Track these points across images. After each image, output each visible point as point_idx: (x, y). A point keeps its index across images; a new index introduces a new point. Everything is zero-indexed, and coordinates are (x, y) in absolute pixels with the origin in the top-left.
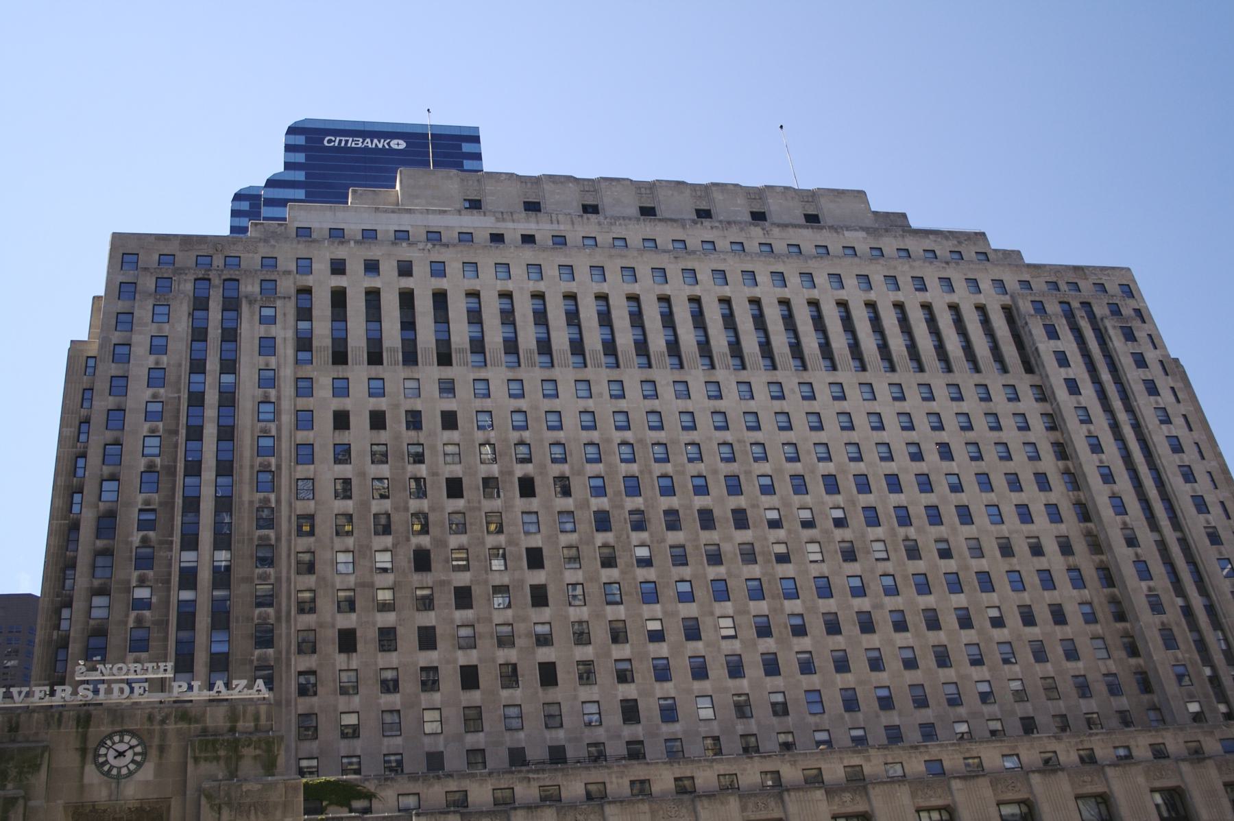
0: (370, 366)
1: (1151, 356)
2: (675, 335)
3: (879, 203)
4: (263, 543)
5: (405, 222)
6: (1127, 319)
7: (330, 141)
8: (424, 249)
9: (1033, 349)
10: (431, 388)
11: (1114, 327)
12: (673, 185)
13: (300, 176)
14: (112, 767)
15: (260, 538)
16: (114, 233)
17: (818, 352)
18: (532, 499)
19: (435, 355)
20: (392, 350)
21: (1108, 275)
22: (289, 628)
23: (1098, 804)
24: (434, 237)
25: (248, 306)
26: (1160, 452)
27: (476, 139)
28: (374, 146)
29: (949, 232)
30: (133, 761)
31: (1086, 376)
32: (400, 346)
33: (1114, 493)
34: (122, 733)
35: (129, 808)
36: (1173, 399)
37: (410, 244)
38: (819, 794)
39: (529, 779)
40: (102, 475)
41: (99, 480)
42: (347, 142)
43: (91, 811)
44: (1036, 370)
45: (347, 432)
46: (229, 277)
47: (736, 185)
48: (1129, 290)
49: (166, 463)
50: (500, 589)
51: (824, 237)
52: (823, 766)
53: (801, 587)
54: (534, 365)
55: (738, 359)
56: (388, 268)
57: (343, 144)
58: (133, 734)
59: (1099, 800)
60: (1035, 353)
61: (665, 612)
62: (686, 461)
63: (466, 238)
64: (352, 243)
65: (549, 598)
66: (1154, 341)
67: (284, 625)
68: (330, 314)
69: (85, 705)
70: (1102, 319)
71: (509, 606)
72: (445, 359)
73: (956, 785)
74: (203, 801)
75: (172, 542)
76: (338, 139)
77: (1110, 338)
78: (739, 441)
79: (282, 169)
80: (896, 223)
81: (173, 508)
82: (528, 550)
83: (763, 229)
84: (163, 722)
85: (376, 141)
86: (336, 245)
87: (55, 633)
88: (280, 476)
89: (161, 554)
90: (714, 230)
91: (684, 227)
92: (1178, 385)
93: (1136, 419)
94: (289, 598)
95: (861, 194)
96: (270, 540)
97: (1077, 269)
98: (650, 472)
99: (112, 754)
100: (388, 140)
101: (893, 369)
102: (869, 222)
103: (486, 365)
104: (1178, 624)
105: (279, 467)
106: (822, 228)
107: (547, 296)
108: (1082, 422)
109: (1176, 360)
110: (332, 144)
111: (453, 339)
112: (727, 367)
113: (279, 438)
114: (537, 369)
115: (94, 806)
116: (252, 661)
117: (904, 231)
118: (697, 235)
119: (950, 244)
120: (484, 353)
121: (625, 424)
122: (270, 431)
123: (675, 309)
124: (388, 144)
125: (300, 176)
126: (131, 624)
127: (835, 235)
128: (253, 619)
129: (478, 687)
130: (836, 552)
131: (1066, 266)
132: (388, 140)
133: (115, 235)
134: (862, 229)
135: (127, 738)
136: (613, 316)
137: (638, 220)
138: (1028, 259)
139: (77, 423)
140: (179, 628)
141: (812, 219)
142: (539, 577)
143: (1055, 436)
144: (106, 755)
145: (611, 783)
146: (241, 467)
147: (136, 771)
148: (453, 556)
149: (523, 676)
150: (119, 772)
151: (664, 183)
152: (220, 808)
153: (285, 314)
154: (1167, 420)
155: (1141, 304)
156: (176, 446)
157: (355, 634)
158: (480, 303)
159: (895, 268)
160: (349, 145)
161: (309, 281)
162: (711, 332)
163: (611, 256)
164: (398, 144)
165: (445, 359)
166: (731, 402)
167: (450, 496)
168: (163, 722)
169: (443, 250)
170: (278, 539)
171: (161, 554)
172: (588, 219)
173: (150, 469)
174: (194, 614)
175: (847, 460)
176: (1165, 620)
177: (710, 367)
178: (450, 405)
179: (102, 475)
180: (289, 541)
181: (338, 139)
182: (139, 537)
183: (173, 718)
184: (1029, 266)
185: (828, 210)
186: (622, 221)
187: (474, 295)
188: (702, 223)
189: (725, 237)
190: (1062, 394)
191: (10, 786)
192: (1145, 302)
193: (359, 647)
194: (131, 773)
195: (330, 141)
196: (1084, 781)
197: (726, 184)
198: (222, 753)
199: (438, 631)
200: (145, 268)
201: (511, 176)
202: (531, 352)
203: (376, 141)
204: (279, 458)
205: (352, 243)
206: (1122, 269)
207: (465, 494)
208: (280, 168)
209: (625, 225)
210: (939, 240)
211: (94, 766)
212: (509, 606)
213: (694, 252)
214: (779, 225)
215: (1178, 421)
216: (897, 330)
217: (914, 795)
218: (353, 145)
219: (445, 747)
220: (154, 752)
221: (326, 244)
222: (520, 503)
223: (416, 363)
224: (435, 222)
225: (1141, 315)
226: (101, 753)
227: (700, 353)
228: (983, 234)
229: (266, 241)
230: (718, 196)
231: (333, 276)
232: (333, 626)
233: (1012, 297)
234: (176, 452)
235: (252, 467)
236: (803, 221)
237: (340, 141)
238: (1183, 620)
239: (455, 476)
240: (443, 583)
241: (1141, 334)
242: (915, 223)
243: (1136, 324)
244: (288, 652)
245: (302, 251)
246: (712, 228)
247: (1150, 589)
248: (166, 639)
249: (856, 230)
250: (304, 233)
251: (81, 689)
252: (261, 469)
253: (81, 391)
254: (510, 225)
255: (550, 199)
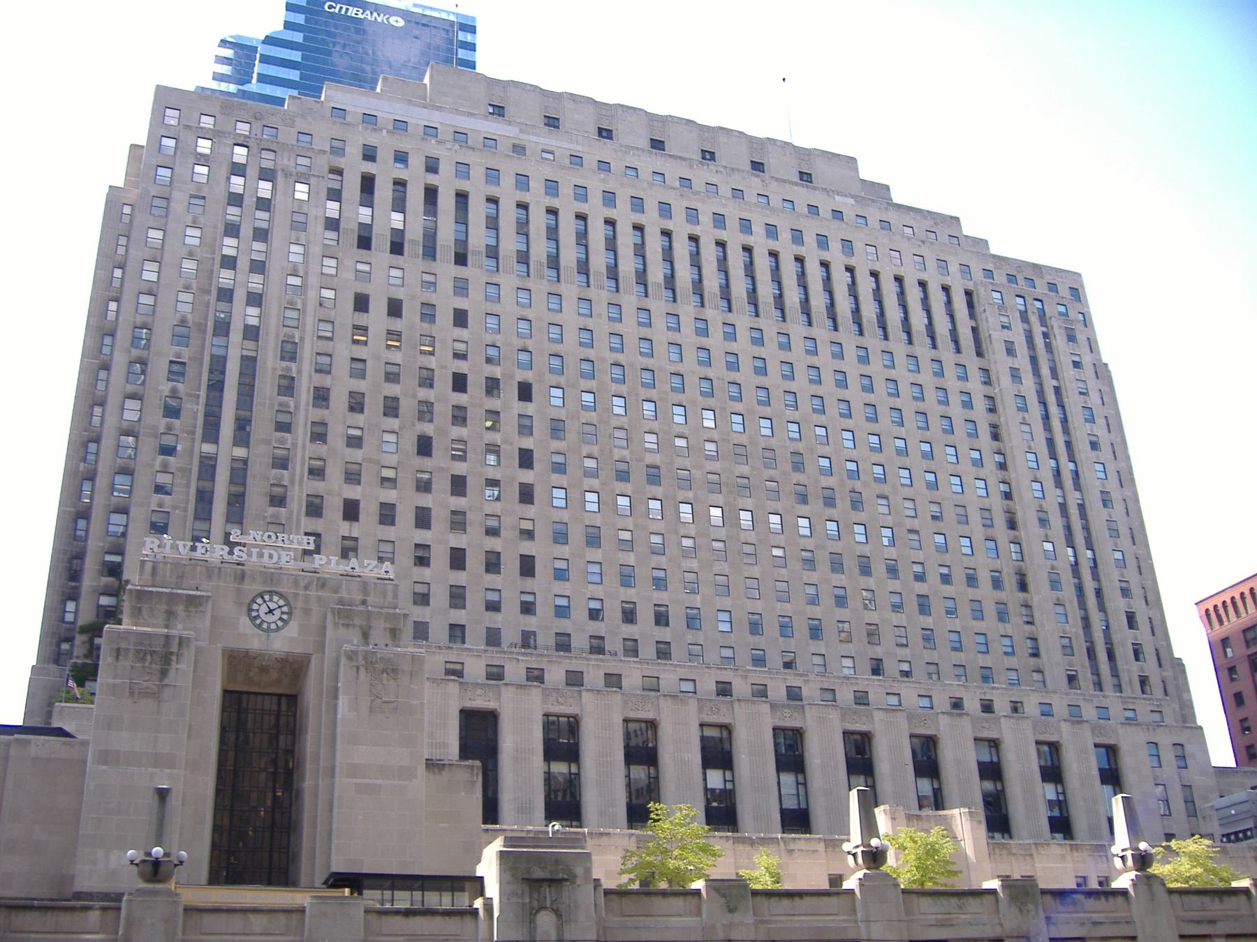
0: (392, 255)
1: (1087, 359)
2: (672, 269)
3: (866, 173)
4: (283, 409)
5: (436, 118)
6: (1071, 322)
7: (330, 7)
8: (451, 149)
9: (987, 335)
10: (446, 285)
11: (1060, 327)
12: (684, 122)
13: (298, 37)
14: (263, 621)
15: (281, 404)
16: (158, 86)
17: (798, 306)
18: (528, 404)
19: (453, 254)
20: (414, 242)
21: (1062, 277)
22: (301, 491)
23: (990, 747)
24: (460, 136)
25: (284, 179)
26: (1080, 448)
27: (472, 30)
28: (373, 19)
29: (928, 211)
30: (281, 619)
31: (1029, 368)
32: (421, 240)
33: (1036, 478)
34: (271, 593)
35: (276, 658)
36: (1099, 401)
37: (439, 142)
38: (765, 708)
39: (518, 659)
40: (135, 322)
41: (132, 326)
42: (347, 9)
43: (244, 656)
44: (986, 355)
45: (366, 315)
46: (265, 147)
47: (741, 133)
48: (1077, 293)
49: (197, 320)
50: (493, 483)
51: (817, 199)
52: (769, 684)
53: (756, 520)
54: (542, 277)
55: (612, 252)
56: (417, 162)
57: (343, 12)
58: (281, 596)
59: (992, 744)
60: (988, 339)
61: (636, 526)
62: (669, 390)
63: (490, 142)
64: (384, 132)
65: (535, 497)
66: (1092, 346)
67: (297, 487)
68: (359, 199)
69: (238, 564)
70: (1050, 318)
71: (498, 499)
72: (461, 259)
73: (878, 716)
74: (343, 660)
75: (198, 396)
76: (339, 6)
77: (1055, 336)
78: (718, 379)
79: (281, 27)
80: (879, 192)
81: (201, 364)
82: (521, 450)
83: (763, 181)
84: (306, 588)
85: (375, 14)
86: (369, 131)
87: (82, 464)
88: (302, 349)
89: (188, 405)
90: (719, 175)
91: (691, 167)
92: (1105, 389)
93: (1065, 414)
94: (303, 464)
95: (852, 161)
96: (289, 407)
97: (1036, 267)
98: (637, 395)
99: (264, 609)
100: (388, 16)
101: (861, 333)
102: (856, 189)
103: (498, 271)
104: (1071, 602)
105: (302, 339)
106: (815, 189)
107: (561, 213)
108: (1019, 409)
109: (1106, 365)
110: (332, 10)
111: (471, 241)
112: (716, 308)
113: (304, 311)
114: (545, 282)
115: (247, 652)
116: (265, 518)
117: (888, 204)
118: (702, 175)
119: (928, 224)
120: (497, 259)
121: (619, 346)
122: (296, 304)
123: (675, 245)
124: (387, 19)
125: (298, 37)
126: (157, 467)
127: (826, 197)
128: (268, 479)
129: (464, 569)
130: (791, 493)
131: (1027, 262)
132: (388, 16)
133: (158, 87)
134: (852, 196)
135: (275, 598)
136: (619, 243)
137: (651, 153)
138: (994, 250)
139: (112, 267)
140: (200, 478)
141: (805, 177)
142: (527, 476)
143: (992, 418)
144: (258, 610)
145: (589, 673)
146: (267, 334)
147: (283, 627)
148: (453, 446)
149: (505, 565)
150: (269, 627)
151: (676, 120)
152: (358, 668)
153: (318, 193)
154: (1091, 420)
155: (1085, 309)
156: (208, 305)
157: (359, 505)
158: (497, 210)
159: (877, 238)
160: (349, 14)
161: (340, 162)
162: (705, 272)
163: (622, 185)
164: (397, 21)
165: (461, 259)
166: (715, 341)
167: (455, 389)
168: (306, 588)
169: (470, 152)
170: (297, 407)
171: (188, 405)
172: (605, 144)
173: (183, 322)
174: (214, 467)
175: (811, 411)
176: (1061, 596)
177: (700, 304)
178: (462, 304)
179: (135, 322)
180: (307, 411)
181: (339, 6)
182: (169, 387)
183: (315, 587)
184: (994, 256)
185: (820, 171)
186: (635, 151)
187: (493, 200)
188: (708, 165)
189: (727, 183)
190: (1006, 380)
191: (180, 626)
192: (1088, 308)
193: (361, 517)
194: (278, 629)
195: (330, 7)
196: (983, 727)
197: (732, 130)
198: (357, 621)
199: (434, 513)
200: (188, 126)
201: (535, 88)
202: (541, 264)
203: (375, 14)
204: (304, 331)
205: (384, 132)
206: (1075, 273)
207: (469, 389)
208: (279, 27)
209: (639, 156)
210: (918, 218)
211: (248, 618)
212: (498, 499)
213: (698, 193)
214: (777, 180)
215: (1101, 422)
216: (871, 297)
217: (843, 719)
218: (353, 15)
219: (431, 618)
220: (298, 613)
221: (360, 129)
222: (518, 407)
223: (434, 258)
224: (464, 123)
225: (1086, 321)
226: (254, 608)
227: (693, 289)
228: (957, 219)
229: (303, 116)
230: (722, 139)
231: (364, 162)
232: (340, 495)
233: (975, 283)
234: (208, 311)
235: (277, 335)
236: (796, 178)
237: (341, 8)
238: (1075, 598)
239: (461, 372)
240: (441, 470)
241: (1081, 338)
242: (897, 198)
243: (1079, 327)
244: (299, 514)
245: (337, 132)
246: (717, 172)
247: (1053, 568)
248: (188, 485)
249: (846, 196)
250: (339, 112)
251: (236, 550)
252: (286, 339)
253: (116, 236)
254: (534, 139)
255: (568, 117)
